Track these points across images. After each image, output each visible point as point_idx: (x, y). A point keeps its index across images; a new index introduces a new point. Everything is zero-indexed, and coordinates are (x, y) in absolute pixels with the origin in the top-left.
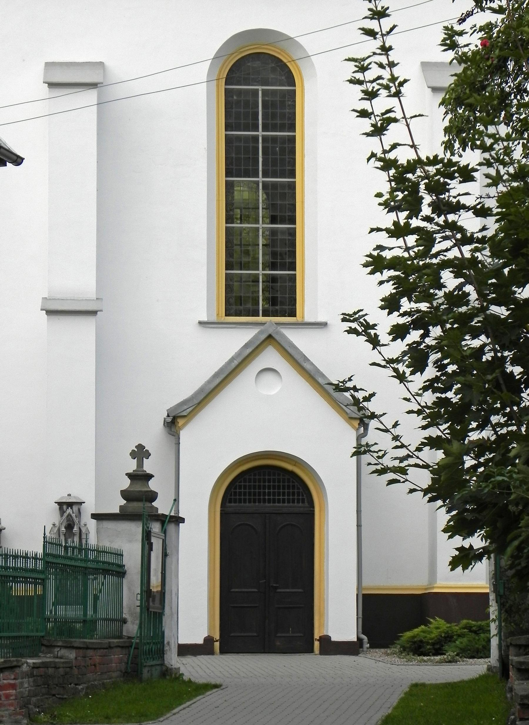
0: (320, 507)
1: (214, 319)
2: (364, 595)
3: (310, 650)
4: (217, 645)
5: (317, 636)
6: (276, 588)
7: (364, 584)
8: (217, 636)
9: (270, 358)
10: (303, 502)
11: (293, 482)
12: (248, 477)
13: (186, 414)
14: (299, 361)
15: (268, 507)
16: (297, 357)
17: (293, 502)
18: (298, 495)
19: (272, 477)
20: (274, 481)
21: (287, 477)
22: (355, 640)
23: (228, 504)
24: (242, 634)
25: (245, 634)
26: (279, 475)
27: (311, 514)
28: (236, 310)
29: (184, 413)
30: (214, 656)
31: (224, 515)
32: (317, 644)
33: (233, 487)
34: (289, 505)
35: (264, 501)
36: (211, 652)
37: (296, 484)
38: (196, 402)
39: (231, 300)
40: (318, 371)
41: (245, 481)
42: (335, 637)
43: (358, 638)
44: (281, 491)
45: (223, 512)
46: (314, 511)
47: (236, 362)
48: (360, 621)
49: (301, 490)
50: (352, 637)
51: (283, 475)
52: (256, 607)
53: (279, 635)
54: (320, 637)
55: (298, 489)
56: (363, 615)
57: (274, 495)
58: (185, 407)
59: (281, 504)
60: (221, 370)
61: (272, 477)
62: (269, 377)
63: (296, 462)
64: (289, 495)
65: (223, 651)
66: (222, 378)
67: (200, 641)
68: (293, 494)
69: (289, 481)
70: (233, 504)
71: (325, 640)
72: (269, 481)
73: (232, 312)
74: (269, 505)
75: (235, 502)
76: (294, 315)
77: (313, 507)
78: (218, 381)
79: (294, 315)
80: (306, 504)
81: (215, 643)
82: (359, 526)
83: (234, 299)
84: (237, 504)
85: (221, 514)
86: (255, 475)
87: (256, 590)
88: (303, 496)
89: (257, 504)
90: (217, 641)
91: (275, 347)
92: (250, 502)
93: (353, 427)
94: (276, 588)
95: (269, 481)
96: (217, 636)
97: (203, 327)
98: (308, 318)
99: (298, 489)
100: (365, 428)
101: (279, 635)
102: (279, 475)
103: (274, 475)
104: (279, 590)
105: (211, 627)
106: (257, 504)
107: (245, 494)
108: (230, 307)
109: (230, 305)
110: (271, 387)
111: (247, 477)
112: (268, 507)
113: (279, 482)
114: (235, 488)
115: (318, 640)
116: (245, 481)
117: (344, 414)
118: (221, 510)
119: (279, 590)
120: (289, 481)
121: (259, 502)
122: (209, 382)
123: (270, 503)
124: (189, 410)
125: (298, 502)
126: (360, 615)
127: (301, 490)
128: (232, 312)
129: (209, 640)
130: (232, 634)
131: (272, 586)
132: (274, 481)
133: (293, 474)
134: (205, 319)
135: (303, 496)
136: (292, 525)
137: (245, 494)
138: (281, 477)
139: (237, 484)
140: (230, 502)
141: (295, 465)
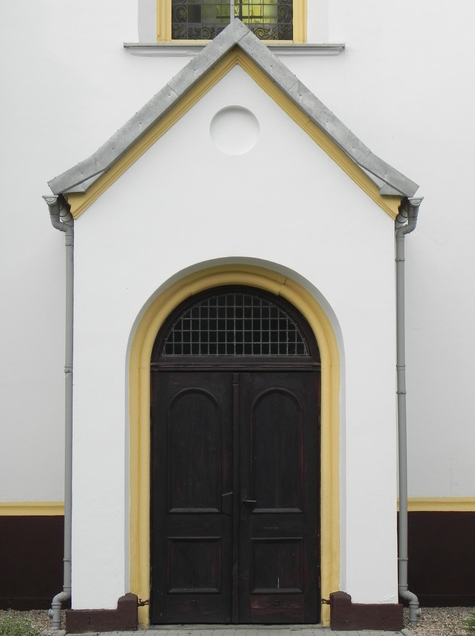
0: (331, 358)
1: (154, 41)
2: (411, 515)
3: (314, 619)
4: (144, 611)
5: (325, 595)
6: (252, 506)
7: (411, 494)
8: (144, 594)
9: (237, 87)
10: (300, 350)
11: (282, 315)
12: (200, 307)
13: (83, 190)
14: (289, 92)
15: (237, 360)
16: (284, 83)
17: (283, 351)
18: (292, 339)
19: (243, 307)
20: (248, 314)
21: (271, 306)
22: (396, 601)
23: (165, 356)
24: (192, 590)
25: (197, 590)
26: (256, 303)
27: (314, 375)
28: (191, 29)
29: (80, 189)
30: (137, 633)
31: (157, 375)
32: (325, 609)
33: (174, 325)
34: (275, 356)
35: (231, 350)
36: (133, 625)
37: (287, 318)
38: (101, 167)
39: (181, 12)
40: (324, 109)
41: (195, 314)
42: (359, 597)
43: (401, 598)
44: (261, 331)
45: (156, 370)
46: (320, 367)
47: (174, 95)
48: (405, 566)
49: (296, 330)
50: (392, 598)
51: (264, 304)
52: (215, 540)
53: (257, 591)
54: (332, 596)
55: (292, 327)
56: (409, 556)
57: (248, 339)
58: (82, 177)
59: (261, 355)
60: (147, 109)
61: (243, 307)
62: (234, 123)
63: (287, 278)
64: (274, 339)
65: (156, 620)
66: (148, 124)
67: (111, 605)
68: (283, 338)
69: (274, 311)
70: (173, 355)
71: (341, 602)
72: (239, 313)
73: (183, 33)
74: (239, 356)
75: (178, 352)
76: (291, 38)
77: (319, 361)
78: (141, 128)
79: (291, 38)
80: (306, 355)
81: (140, 608)
82: (401, 393)
83: (187, 11)
84: (182, 355)
85: (152, 373)
86: (213, 303)
87: (215, 510)
88: (299, 339)
89: (217, 355)
90: (143, 604)
91: (246, 69)
92: (204, 352)
93: (388, 211)
94: (252, 506)
95: (239, 313)
96: (144, 595)
97: (133, 54)
98: (310, 41)
99: (292, 327)
100: (411, 215)
101: (257, 591)
102: (256, 303)
103: (248, 302)
104: (257, 510)
105: (132, 576)
106: (217, 355)
107: (195, 337)
108: (180, 24)
109: (183, 20)
110: (238, 141)
111: (199, 306)
112: (237, 360)
113: (257, 314)
114: (178, 327)
115: (328, 602)
116: (195, 314)
117: (374, 190)
118: (152, 367)
119: (257, 510)
120: (274, 314)
121: (222, 352)
122: (124, 131)
123: (241, 353)
124: (88, 183)
125: (291, 352)
126: (405, 555)
127: (296, 330)
128: (183, 33)
129: (128, 604)
130: (173, 590)
131: (245, 503)
132: (248, 314)
133: (281, 301)
134: (135, 40)
135: (299, 339)
136: (281, 392)
137: (195, 337)
138: (261, 306)
139: (182, 318)
140: (169, 351)
141: (284, 284)
